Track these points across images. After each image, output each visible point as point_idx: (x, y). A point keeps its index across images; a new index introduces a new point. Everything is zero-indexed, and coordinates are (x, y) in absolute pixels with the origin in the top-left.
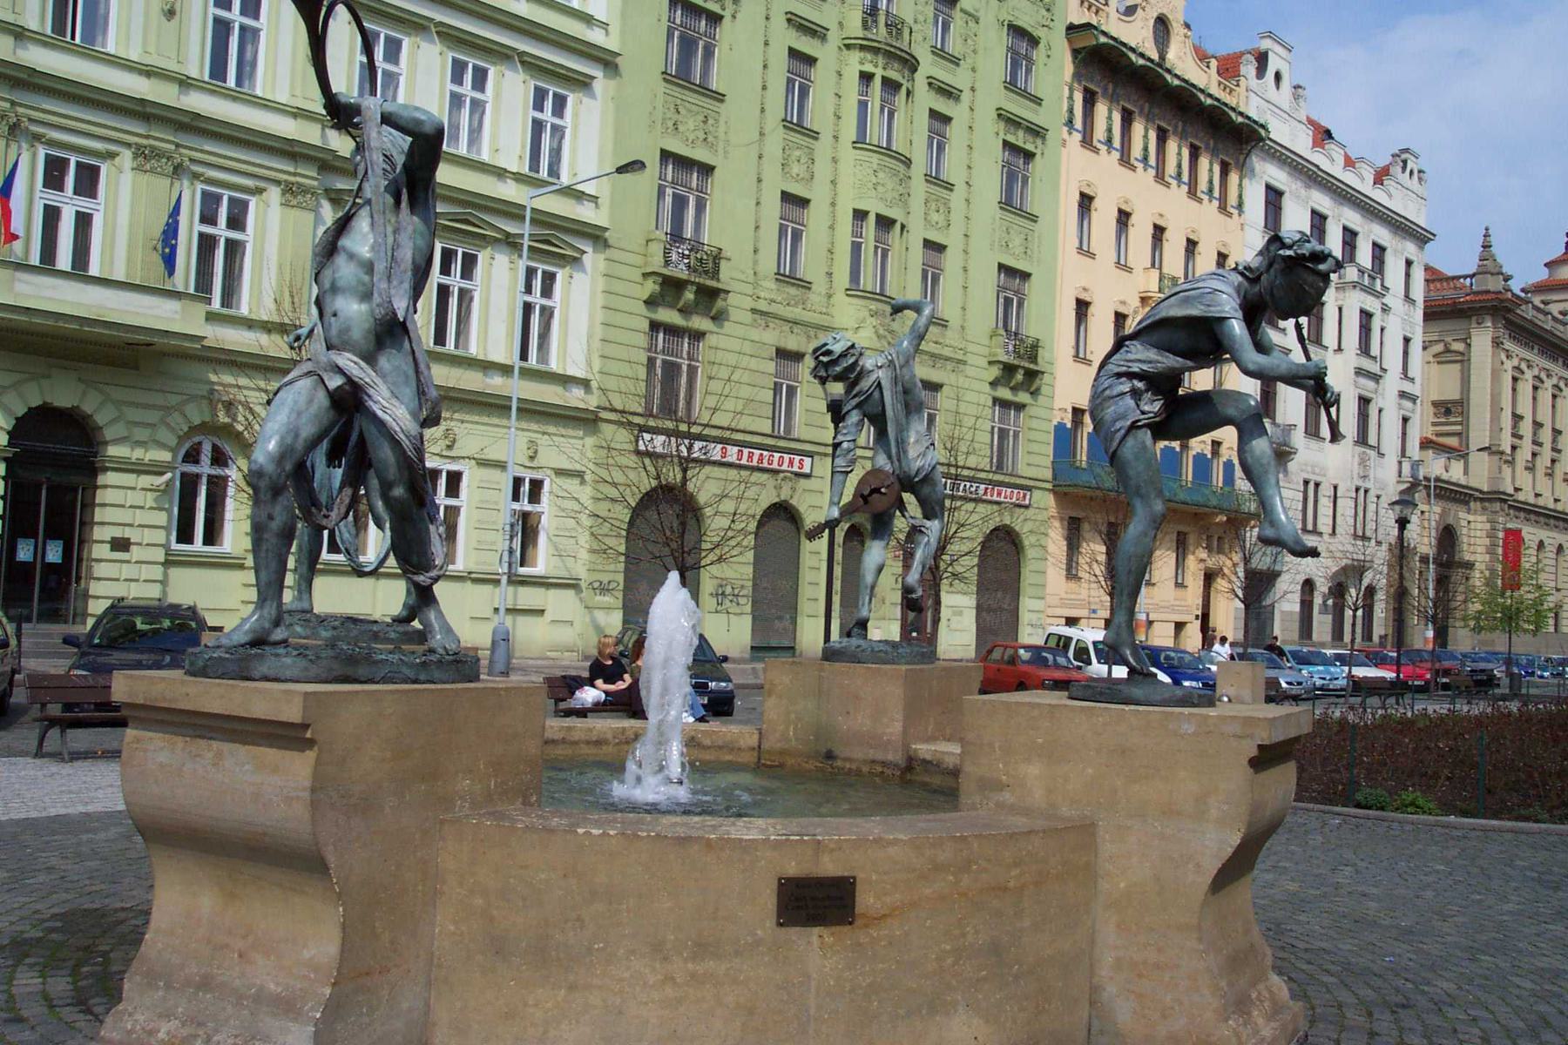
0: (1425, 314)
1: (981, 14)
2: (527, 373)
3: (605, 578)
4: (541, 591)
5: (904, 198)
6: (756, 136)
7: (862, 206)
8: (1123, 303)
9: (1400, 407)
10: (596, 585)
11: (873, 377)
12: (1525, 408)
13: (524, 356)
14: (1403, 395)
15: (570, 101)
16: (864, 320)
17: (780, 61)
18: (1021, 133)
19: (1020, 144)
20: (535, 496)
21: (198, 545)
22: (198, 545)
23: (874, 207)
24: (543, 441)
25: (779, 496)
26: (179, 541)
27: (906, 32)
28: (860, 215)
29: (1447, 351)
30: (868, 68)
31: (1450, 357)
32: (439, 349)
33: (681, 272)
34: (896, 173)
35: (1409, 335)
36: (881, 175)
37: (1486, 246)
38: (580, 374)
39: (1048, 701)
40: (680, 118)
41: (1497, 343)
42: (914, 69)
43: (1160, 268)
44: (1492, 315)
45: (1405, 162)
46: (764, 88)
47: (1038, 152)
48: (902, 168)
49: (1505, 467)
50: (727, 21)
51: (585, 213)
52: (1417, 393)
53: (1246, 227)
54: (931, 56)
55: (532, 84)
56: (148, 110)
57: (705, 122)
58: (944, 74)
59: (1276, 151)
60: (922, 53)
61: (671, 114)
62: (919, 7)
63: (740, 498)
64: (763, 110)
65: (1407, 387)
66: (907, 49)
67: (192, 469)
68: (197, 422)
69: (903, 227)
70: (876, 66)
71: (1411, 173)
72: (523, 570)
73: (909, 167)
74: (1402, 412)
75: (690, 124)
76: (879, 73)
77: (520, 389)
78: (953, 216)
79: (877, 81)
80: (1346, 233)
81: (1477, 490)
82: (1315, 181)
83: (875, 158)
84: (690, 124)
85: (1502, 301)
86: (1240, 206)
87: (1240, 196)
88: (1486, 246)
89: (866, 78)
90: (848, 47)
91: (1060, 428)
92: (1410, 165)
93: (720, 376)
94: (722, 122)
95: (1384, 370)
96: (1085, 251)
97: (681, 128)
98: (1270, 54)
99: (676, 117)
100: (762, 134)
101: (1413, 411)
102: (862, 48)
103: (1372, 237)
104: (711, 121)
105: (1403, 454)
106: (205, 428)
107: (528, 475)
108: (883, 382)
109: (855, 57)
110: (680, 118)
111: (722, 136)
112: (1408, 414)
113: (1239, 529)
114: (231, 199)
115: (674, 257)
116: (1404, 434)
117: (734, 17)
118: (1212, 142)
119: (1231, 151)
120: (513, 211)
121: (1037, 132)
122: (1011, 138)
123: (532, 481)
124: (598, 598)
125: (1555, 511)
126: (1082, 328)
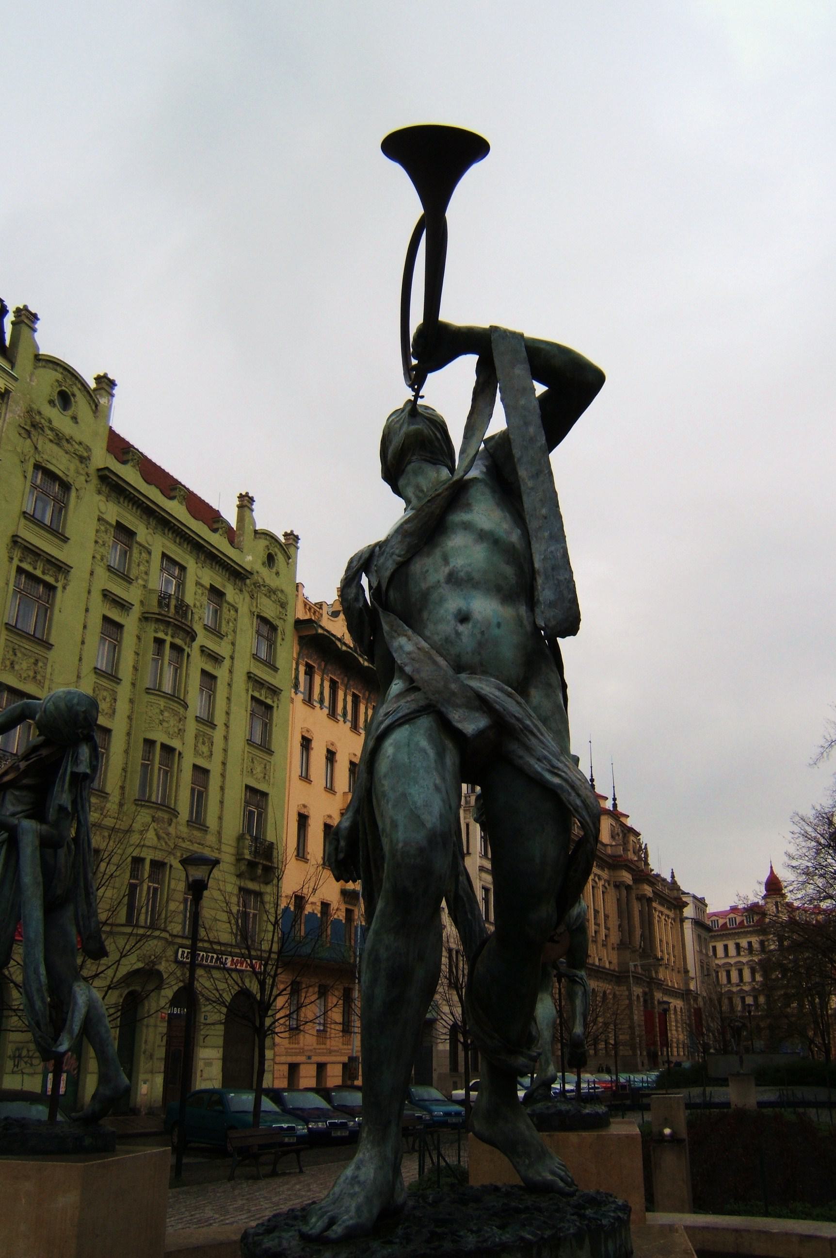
58: (211, 645)
60: (198, 628)
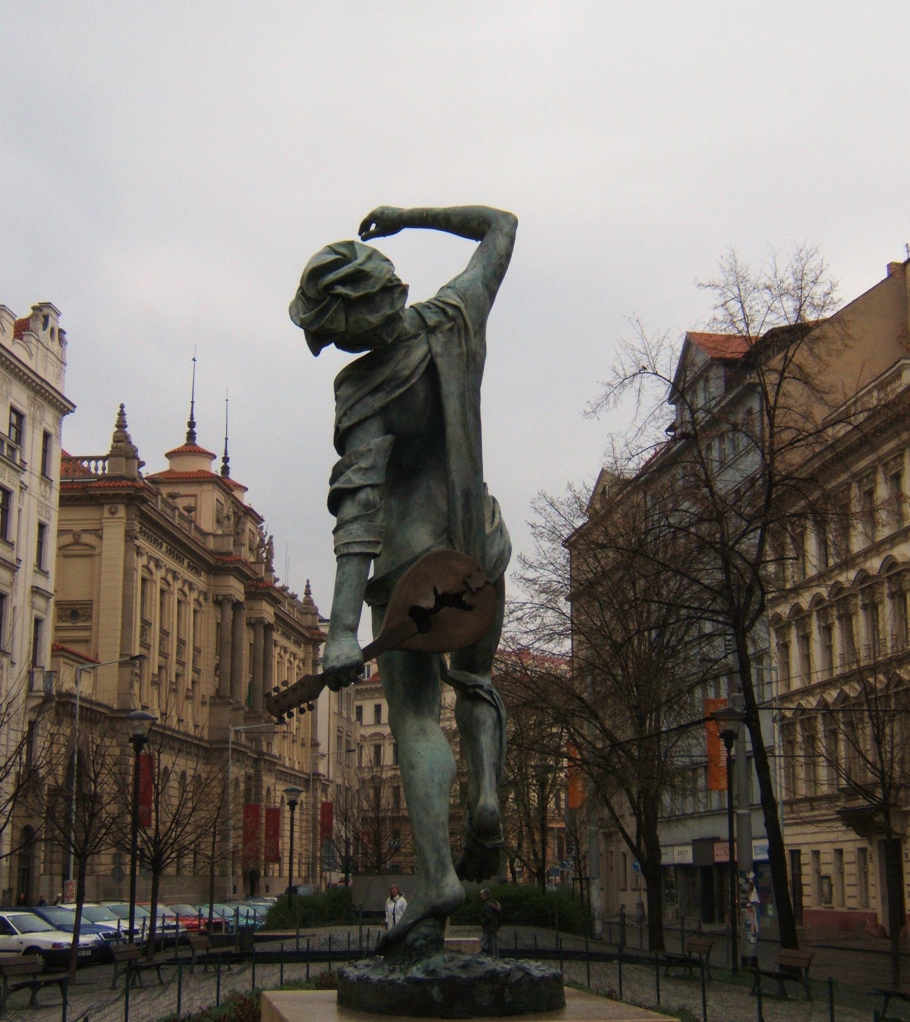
0: (61, 498)
9: (33, 606)
11: (419, 353)
12: (154, 617)
14: (36, 591)
29: (77, 542)
31: (76, 550)
35: (45, 521)
37: (121, 425)
41: (130, 536)
44: (127, 506)
45: (46, 318)
49: (135, 679)
52: (51, 590)
63: (663, 626)
65: (41, 582)
71: (52, 330)
74: (35, 612)
81: (106, 707)
85: (138, 489)
88: (121, 425)
92: (51, 322)
95: (19, 560)
101: (46, 611)
103: (11, 400)
105: (34, 662)
108: (441, 363)
112: (41, 615)
116: (36, 639)
125: (178, 732)
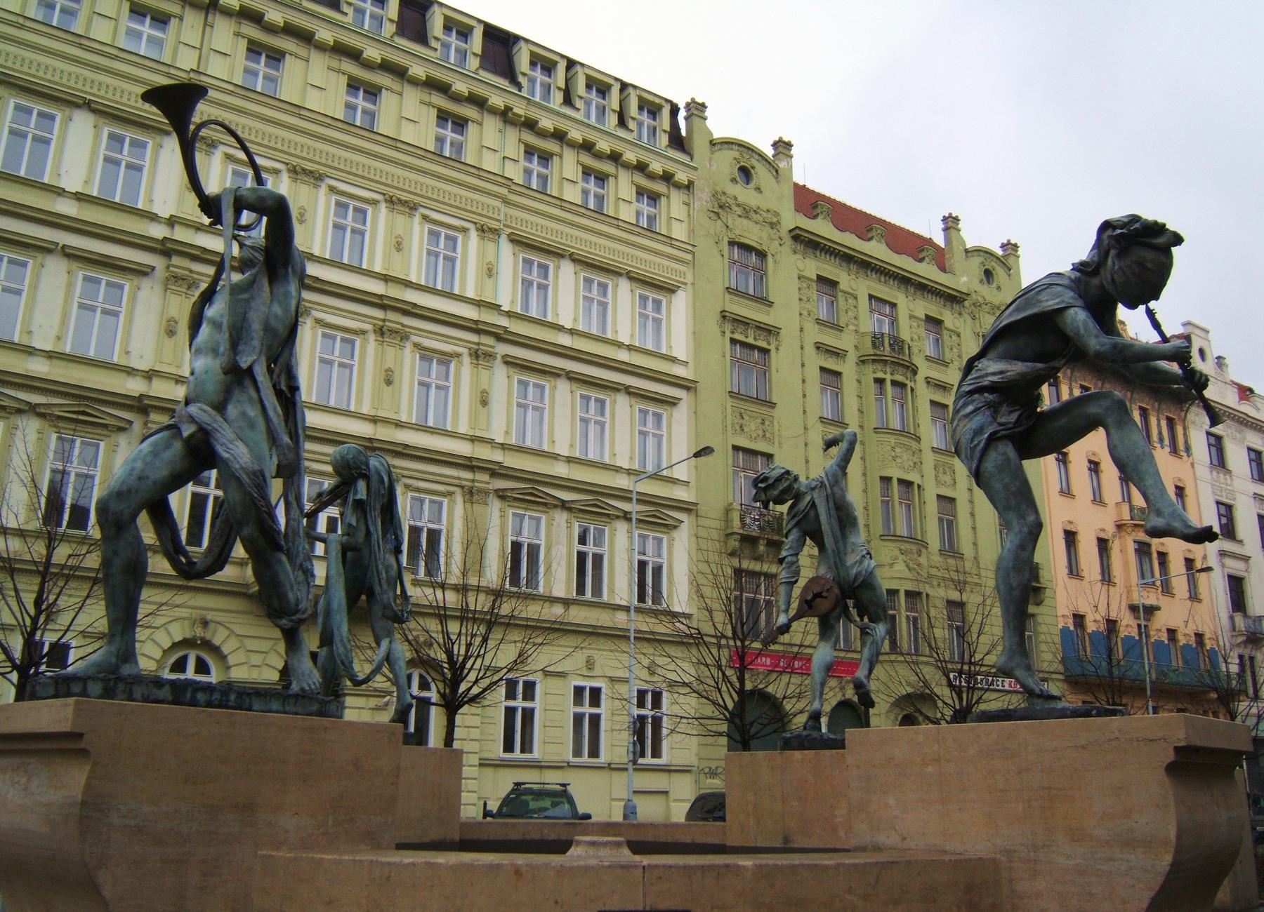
1: (961, 330)
2: (433, 585)
3: (713, 765)
4: (664, 776)
5: (918, 465)
6: (803, 431)
7: (887, 473)
8: (1103, 530)
10: (707, 770)
13: (642, 598)
15: (608, 403)
16: (896, 558)
17: (814, 375)
18: (751, 332)
19: (750, 340)
20: (657, 703)
21: (517, 754)
22: (517, 754)
23: (895, 473)
24: (596, 655)
25: (844, 695)
26: (574, 756)
27: (906, 347)
28: (886, 480)
30: (880, 375)
32: (641, 605)
33: (754, 531)
34: (908, 448)
36: (898, 450)
38: (624, 603)
39: (862, 861)
40: (744, 422)
42: (915, 373)
43: (1130, 501)
46: (804, 396)
47: (772, 348)
48: (914, 444)
50: (773, 353)
51: (681, 494)
53: (1196, 465)
54: (817, 327)
55: (637, 407)
56: (375, 445)
57: (763, 424)
59: (1230, 414)
60: (919, 361)
61: (738, 420)
62: (914, 330)
64: (805, 412)
66: (907, 359)
67: (511, 703)
68: (178, 638)
69: (919, 486)
70: (885, 373)
72: (641, 761)
73: (919, 443)
75: (752, 426)
76: (888, 377)
77: (578, 615)
78: (958, 478)
79: (888, 383)
80: (1251, 453)
82: (1246, 425)
83: (892, 440)
84: (752, 426)
86: (1188, 449)
87: (1186, 442)
89: (880, 382)
90: (863, 362)
91: (1064, 631)
93: (1230, 666)
94: (775, 423)
96: (1066, 492)
97: (746, 429)
98: (1193, 337)
99: (741, 421)
100: (806, 429)
102: (874, 361)
104: (767, 423)
106: (187, 643)
107: (588, 684)
109: (869, 369)
110: (744, 422)
111: (776, 432)
113: (1228, 704)
114: (595, 528)
115: (748, 521)
117: (777, 349)
118: (1157, 404)
119: (1173, 409)
120: (624, 495)
121: (769, 331)
122: (738, 336)
123: (525, 683)
124: (709, 781)
126: (1072, 552)
